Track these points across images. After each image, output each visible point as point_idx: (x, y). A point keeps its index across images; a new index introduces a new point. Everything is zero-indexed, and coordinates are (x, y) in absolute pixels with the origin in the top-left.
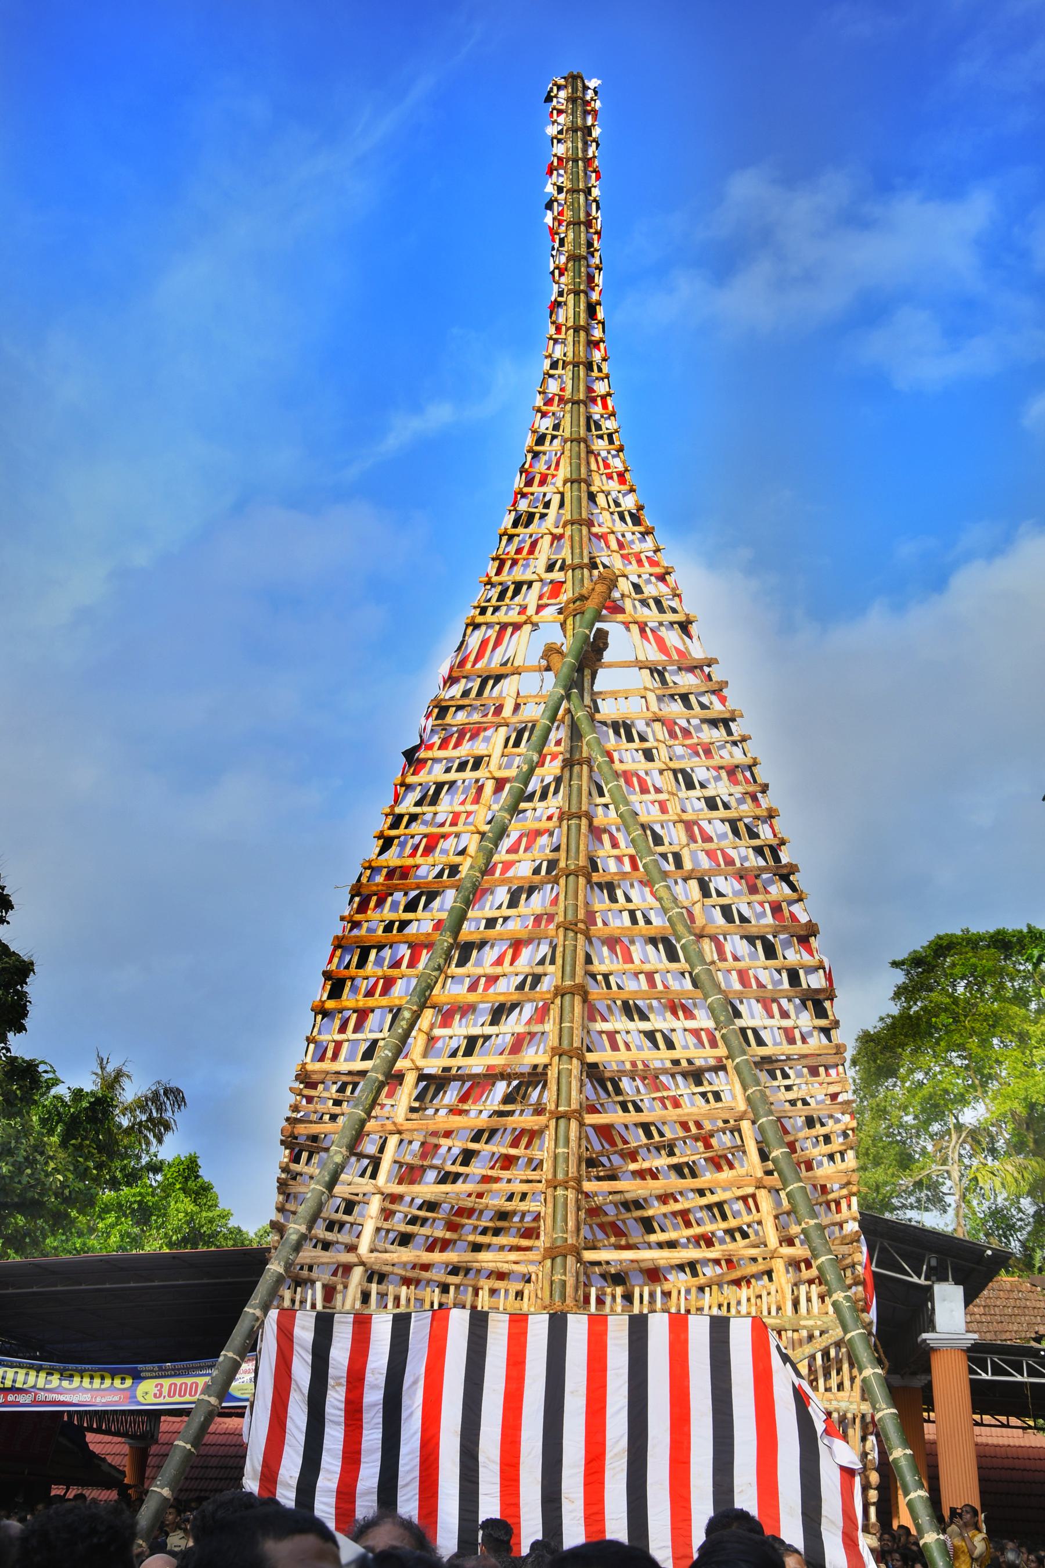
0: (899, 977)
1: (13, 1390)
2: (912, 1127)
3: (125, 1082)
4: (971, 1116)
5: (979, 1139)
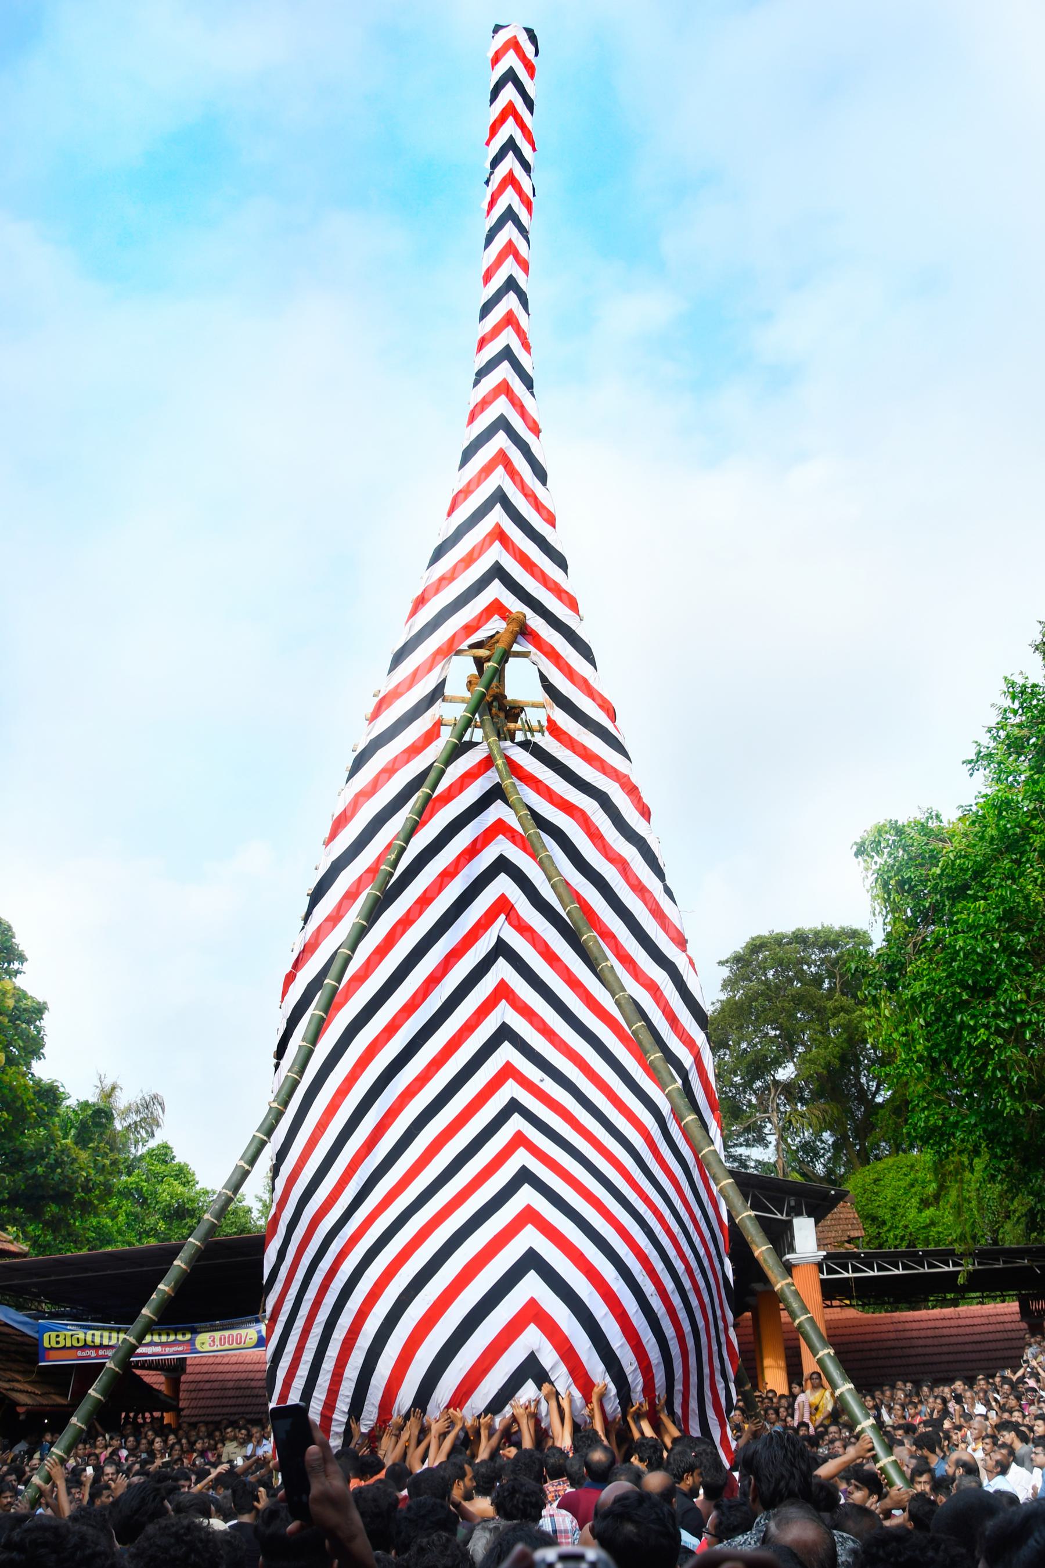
0: (725, 972)
1: (101, 1346)
2: (740, 1085)
3: (118, 1093)
4: (786, 1073)
5: (788, 1090)
